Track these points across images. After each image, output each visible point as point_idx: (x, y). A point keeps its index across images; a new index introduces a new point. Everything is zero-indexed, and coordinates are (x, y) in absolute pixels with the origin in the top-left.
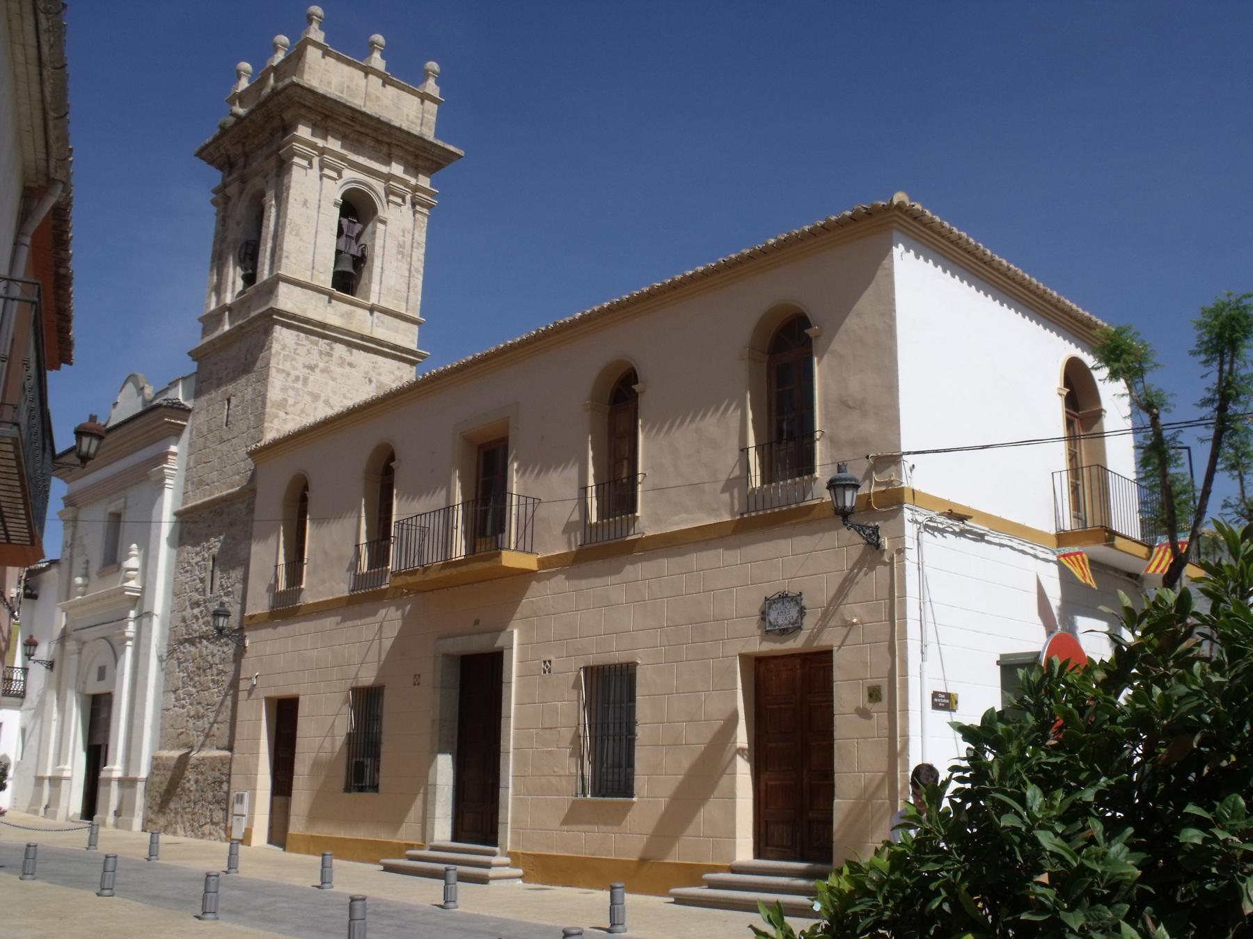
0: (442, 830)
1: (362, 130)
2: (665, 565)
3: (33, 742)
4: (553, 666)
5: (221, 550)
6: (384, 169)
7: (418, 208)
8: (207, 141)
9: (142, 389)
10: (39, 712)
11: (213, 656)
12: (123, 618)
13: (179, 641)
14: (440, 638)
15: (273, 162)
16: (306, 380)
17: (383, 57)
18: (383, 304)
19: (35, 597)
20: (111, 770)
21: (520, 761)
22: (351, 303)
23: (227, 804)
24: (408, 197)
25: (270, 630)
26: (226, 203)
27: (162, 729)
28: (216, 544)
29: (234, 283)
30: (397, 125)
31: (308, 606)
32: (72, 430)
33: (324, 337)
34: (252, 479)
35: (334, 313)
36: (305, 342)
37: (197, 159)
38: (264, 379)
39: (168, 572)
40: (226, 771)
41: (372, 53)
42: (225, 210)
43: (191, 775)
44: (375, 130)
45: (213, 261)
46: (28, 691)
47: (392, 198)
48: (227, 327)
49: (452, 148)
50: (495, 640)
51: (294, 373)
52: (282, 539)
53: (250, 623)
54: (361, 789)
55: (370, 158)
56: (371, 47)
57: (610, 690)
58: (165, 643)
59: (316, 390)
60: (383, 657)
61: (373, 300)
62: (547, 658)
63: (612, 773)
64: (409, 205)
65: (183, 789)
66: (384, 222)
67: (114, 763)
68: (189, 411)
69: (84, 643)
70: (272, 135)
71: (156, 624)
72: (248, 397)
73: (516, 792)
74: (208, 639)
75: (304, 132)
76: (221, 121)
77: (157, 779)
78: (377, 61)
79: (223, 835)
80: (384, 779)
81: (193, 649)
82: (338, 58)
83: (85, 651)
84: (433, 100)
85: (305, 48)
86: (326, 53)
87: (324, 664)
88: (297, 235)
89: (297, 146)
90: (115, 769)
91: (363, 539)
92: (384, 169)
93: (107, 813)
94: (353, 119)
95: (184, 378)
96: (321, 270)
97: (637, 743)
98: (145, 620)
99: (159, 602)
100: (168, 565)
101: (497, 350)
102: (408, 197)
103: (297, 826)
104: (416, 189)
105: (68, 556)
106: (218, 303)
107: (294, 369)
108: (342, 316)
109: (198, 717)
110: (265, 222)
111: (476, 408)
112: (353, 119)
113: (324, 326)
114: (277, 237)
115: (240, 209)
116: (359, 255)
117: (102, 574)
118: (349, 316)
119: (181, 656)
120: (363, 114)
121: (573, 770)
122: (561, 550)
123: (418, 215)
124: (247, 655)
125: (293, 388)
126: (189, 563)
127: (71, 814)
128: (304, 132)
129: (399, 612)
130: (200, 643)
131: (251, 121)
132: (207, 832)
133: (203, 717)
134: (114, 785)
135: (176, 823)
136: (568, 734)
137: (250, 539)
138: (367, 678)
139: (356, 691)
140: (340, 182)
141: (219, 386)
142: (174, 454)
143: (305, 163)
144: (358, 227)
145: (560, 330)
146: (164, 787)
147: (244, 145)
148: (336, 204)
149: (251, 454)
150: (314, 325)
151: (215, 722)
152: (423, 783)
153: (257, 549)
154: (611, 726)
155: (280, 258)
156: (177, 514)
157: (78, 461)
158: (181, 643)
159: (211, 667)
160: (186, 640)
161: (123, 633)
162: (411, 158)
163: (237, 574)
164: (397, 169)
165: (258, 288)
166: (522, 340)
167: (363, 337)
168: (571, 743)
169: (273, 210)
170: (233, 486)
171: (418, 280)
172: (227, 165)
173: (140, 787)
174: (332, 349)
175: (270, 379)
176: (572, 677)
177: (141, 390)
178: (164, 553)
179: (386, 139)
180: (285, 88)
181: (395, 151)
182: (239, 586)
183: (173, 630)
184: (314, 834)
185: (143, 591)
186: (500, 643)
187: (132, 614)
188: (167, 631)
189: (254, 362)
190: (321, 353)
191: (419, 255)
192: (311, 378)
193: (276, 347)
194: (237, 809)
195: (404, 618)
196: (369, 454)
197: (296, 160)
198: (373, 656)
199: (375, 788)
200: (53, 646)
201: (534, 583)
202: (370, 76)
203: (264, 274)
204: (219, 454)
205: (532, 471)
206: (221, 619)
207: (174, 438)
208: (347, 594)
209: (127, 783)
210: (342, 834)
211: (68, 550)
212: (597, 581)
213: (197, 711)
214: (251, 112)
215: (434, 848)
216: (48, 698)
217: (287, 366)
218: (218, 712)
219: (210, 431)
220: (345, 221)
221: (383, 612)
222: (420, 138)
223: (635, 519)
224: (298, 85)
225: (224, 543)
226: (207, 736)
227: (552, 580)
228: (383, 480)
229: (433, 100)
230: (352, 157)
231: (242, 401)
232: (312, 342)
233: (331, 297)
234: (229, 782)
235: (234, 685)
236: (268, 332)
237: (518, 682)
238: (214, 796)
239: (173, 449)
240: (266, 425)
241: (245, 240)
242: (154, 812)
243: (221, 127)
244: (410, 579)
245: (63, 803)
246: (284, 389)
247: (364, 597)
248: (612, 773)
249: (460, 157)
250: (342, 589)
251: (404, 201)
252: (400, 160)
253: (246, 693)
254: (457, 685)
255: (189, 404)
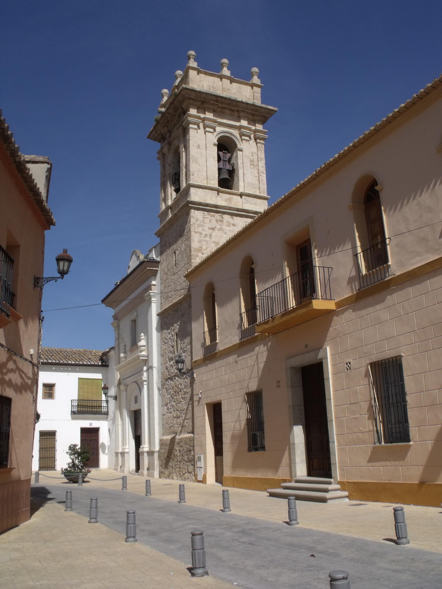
0: (301, 469)
1: (223, 106)
2: (411, 291)
3: (113, 436)
4: (352, 366)
5: (179, 329)
6: (237, 124)
7: (258, 141)
8: (151, 130)
9: (139, 257)
10: (114, 421)
11: (181, 384)
12: (141, 372)
13: (166, 379)
14: (288, 358)
15: (180, 130)
16: (211, 236)
17: (228, 69)
18: (247, 191)
19: (107, 366)
20: (143, 448)
21: (340, 424)
22: (230, 193)
23: (194, 462)
24: (252, 136)
25: (205, 367)
26: (164, 157)
27: (163, 425)
28: (177, 327)
29: (171, 195)
30: (240, 100)
31: (221, 351)
32: (55, 259)
33: (218, 212)
34: (189, 289)
35: (222, 200)
36: (207, 216)
37: (148, 139)
38: (189, 239)
39: (158, 345)
40: (192, 445)
41: (223, 68)
42: (164, 161)
43: (177, 448)
44: (229, 104)
45: (161, 186)
46: (109, 411)
47: (243, 137)
48: (170, 216)
49: (271, 107)
50: (317, 355)
51: (204, 233)
52: (205, 318)
53: (196, 365)
54: (256, 450)
55: (229, 120)
56: (222, 65)
57: (388, 376)
58: (160, 381)
59: (217, 240)
60: (260, 375)
61: (241, 190)
62: (348, 361)
63: (396, 430)
64: (253, 140)
65: (174, 456)
66: (241, 150)
67: (145, 444)
68: (159, 262)
69: (127, 386)
70: (179, 118)
71: (155, 372)
72: (183, 249)
73: (340, 445)
74: (178, 376)
75: (193, 111)
76: (155, 117)
77: (163, 451)
78: (226, 72)
79: (194, 479)
80: (267, 443)
81: (172, 382)
82: (206, 74)
83: (128, 389)
84: (258, 86)
85: (188, 72)
86: (199, 72)
87: (231, 382)
88: (196, 163)
89: (190, 119)
90: (145, 447)
91: (243, 310)
92: (237, 124)
93: (143, 469)
94: (217, 101)
95: (155, 247)
96: (211, 178)
97: (408, 407)
98: (150, 370)
99: (155, 361)
100: (158, 342)
101: (297, 188)
102: (252, 136)
103: (227, 472)
104: (255, 131)
105: (117, 344)
106: (165, 206)
107: (204, 230)
108: (226, 200)
109: (178, 417)
110: (181, 160)
111: (289, 226)
112: (217, 101)
113: (216, 206)
114: (187, 166)
115: (170, 158)
116: (231, 169)
117: (131, 351)
118: (230, 200)
119: (167, 386)
120: (222, 97)
121: (371, 428)
122: (347, 294)
123: (258, 144)
124: (195, 382)
125: (205, 241)
126: (166, 339)
127: (131, 470)
128: (193, 111)
129: (266, 347)
130: (175, 379)
131: (169, 113)
132: (187, 477)
133: (180, 417)
134: (146, 455)
135: (173, 473)
136: (365, 406)
137: (191, 321)
138: (253, 387)
139: (249, 394)
140: (215, 134)
141: (170, 247)
142: (155, 285)
143: (196, 127)
144: (228, 155)
145: (329, 166)
146: (166, 455)
147: (167, 126)
148: (215, 145)
149: (186, 276)
150: (211, 207)
151: (185, 419)
152: (287, 443)
153: (195, 326)
154: (391, 397)
155: (189, 175)
156: (158, 315)
157: (59, 275)
158: (167, 380)
159: (181, 391)
160: (169, 378)
161: (142, 379)
162: (250, 117)
163: (187, 340)
164: (244, 123)
165: (182, 193)
166: (309, 179)
167: (238, 210)
168: (368, 411)
169: (184, 154)
170: (181, 295)
171: (264, 177)
172: (162, 139)
173: (156, 455)
174: (222, 218)
175: (192, 237)
176: (363, 370)
177: (138, 257)
178: (155, 335)
179: (236, 109)
180: (180, 92)
181: (242, 114)
182: (189, 347)
183: (163, 374)
184: (236, 476)
185: (148, 356)
186: (320, 356)
187: (145, 368)
188: (160, 375)
189: (184, 230)
190: (217, 221)
191: (262, 164)
192: (214, 234)
193: (193, 221)
194: (199, 464)
195: (268, 350)
196: (240, 264)
197: (191, 126)
198: (255, 374)
199: (263, 448)
200: (116, 388)
201: (335, 318)
202: (223, 80)
203: (184, 185)
204: (173, 281)
205: (326, 251)
206: (180, 364)
207: (153, 277)
208: (238, 342)
209: (151, 453)
210: (249, 475)
211: (117, 341)
212: (371, 309)
213: (177, 414)
214: (167, 109)
215: (297, 481)
216: (116, 414)
217: (200, 229)
218: (186, 413)
219: (169, 270)
220: (221, 153)
221: (257, 348)
222: (253, 105)
223: (389, 266)
224: (186, 89)
225: (180, 326)
226: (182, 427)
227: (345, 314)
228: (249, 275)
229: (258, 86)
230: (219, 120)
231: (181, 252)
232: (211, 216)
233: (219, 192)
234: (194, 450)
235: (192, 399)
236: (188, 214)
237: (333, 378)
238: (188, 458)
239: (154, 282)
240: (192, 261)
241: (173, 173)
242: (163, 468)
243: (156, 120)
244: (266, 326)
245: (126, 465)
246: (200, 242)
247: (247, 342)
248: (396, 430)
249: (276, 111)
250: (235, 339)
251: (250, 138)
252: (245, 118)
253: (197, 402)
254: (301, 384)
255: (158, 259)
